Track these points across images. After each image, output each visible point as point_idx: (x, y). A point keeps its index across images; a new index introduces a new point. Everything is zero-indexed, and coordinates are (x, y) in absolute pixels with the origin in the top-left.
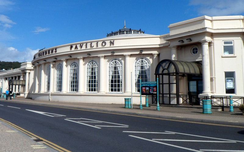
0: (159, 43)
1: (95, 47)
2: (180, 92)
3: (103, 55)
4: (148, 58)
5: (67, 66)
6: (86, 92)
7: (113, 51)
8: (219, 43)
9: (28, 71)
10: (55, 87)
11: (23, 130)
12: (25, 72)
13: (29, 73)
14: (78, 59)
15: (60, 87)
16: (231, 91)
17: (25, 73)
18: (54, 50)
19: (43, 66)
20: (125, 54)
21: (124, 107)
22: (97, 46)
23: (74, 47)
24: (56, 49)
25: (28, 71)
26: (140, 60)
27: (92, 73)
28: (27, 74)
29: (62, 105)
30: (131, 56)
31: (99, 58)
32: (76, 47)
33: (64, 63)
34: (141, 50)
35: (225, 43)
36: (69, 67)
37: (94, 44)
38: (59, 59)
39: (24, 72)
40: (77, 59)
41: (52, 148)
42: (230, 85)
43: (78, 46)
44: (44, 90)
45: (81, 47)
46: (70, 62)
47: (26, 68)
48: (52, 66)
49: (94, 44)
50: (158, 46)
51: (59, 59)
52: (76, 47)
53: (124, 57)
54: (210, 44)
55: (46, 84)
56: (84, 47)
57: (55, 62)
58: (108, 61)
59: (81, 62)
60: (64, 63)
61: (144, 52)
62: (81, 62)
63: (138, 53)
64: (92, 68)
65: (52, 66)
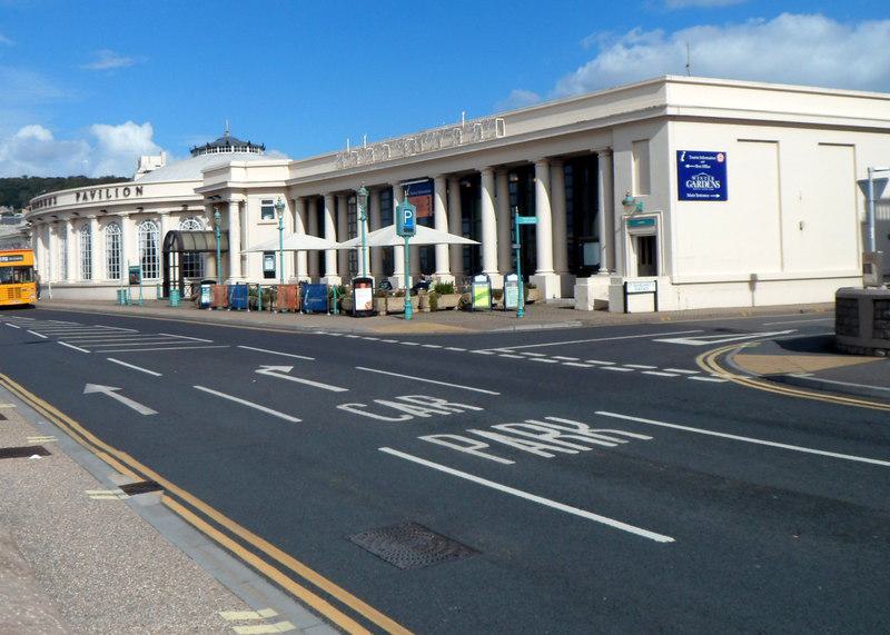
0: (288, 178)
1: (113, 198)
2: (749, 304)
3: (127, 213)
4: (200, 217)
5: (74, 231)
6: (105, 279)
7: (141, 207)
8: (254, 203)
9: (236, 197)
10: (80, 270)
11: (87, 440)
12: (223, 199)
13: (242, 204)
14: (89, 220)
15: (88, 272)
16: (269, 274)
17: (224, 206)
18: (53, 200)
19: (39, 229)
20: (159, 210)
21: (117, 303)
22: (117, 196)
23: (82, 194)
24: (55, 198)
25: (236, 197)
26: (188, 221)
27: (149, 243)
28: (234, 209)
29: (68, 306)
30: (171, 214)
31: (120, 217)
32: (85, 197)
33: (70, 227)
34: (185, 204)
35: (264, 202)
36: (78, 233)
37: (112, 192)
38: (82, 214)
39: (217, 200)
40: (86, 218)
41: (175, 513)
42: (269, 267)
43: (88, 194)
44: (75, 276)
45: (93, 196)
46: (78, 224)
47: (229, 185)
48: (51, 230)
49: (112, 192)
50: (284, 184)
51: (82, 214)
52: (85, 197)
53: (159, 216)
54: (242, 204)
55: (61, 264)
56: (97, 198)
57: (56, 222)
58: (137, 224)
59: (95, 224)
60: (70, 227)
61: (190, 208)
62: (95, 224)
63: (181, 209)
64: (149, 234)
65: (51, 230)
